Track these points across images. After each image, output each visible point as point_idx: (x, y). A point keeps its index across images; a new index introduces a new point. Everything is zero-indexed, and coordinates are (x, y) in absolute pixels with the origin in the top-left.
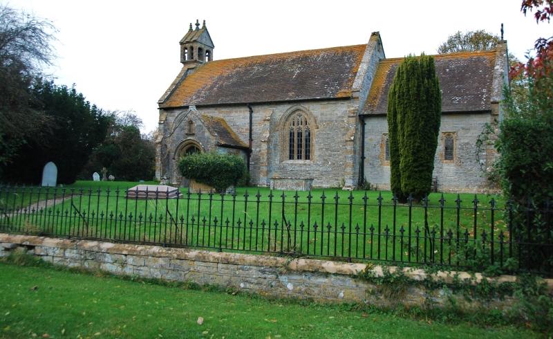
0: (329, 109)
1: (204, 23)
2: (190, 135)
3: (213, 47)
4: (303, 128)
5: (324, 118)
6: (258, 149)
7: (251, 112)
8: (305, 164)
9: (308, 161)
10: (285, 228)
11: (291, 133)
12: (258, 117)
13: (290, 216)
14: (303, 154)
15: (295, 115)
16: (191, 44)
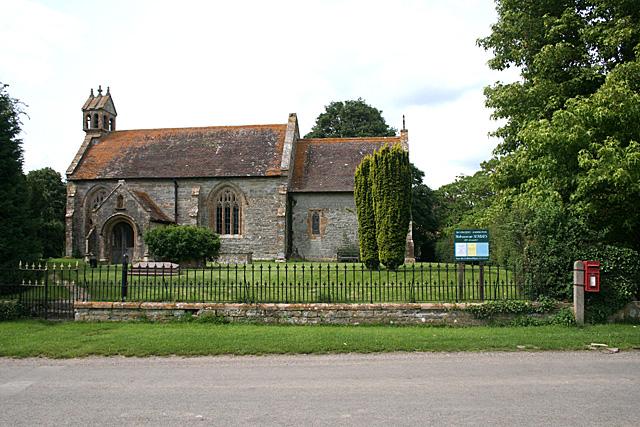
4: (231, 205)
7: (177, 187)
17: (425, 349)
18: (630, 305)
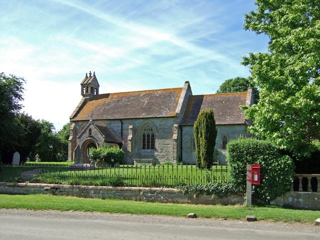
1: (94, 74)
4: (150, 133)
7: (122, 123)
17: (6, 194)
18: (288, 194)
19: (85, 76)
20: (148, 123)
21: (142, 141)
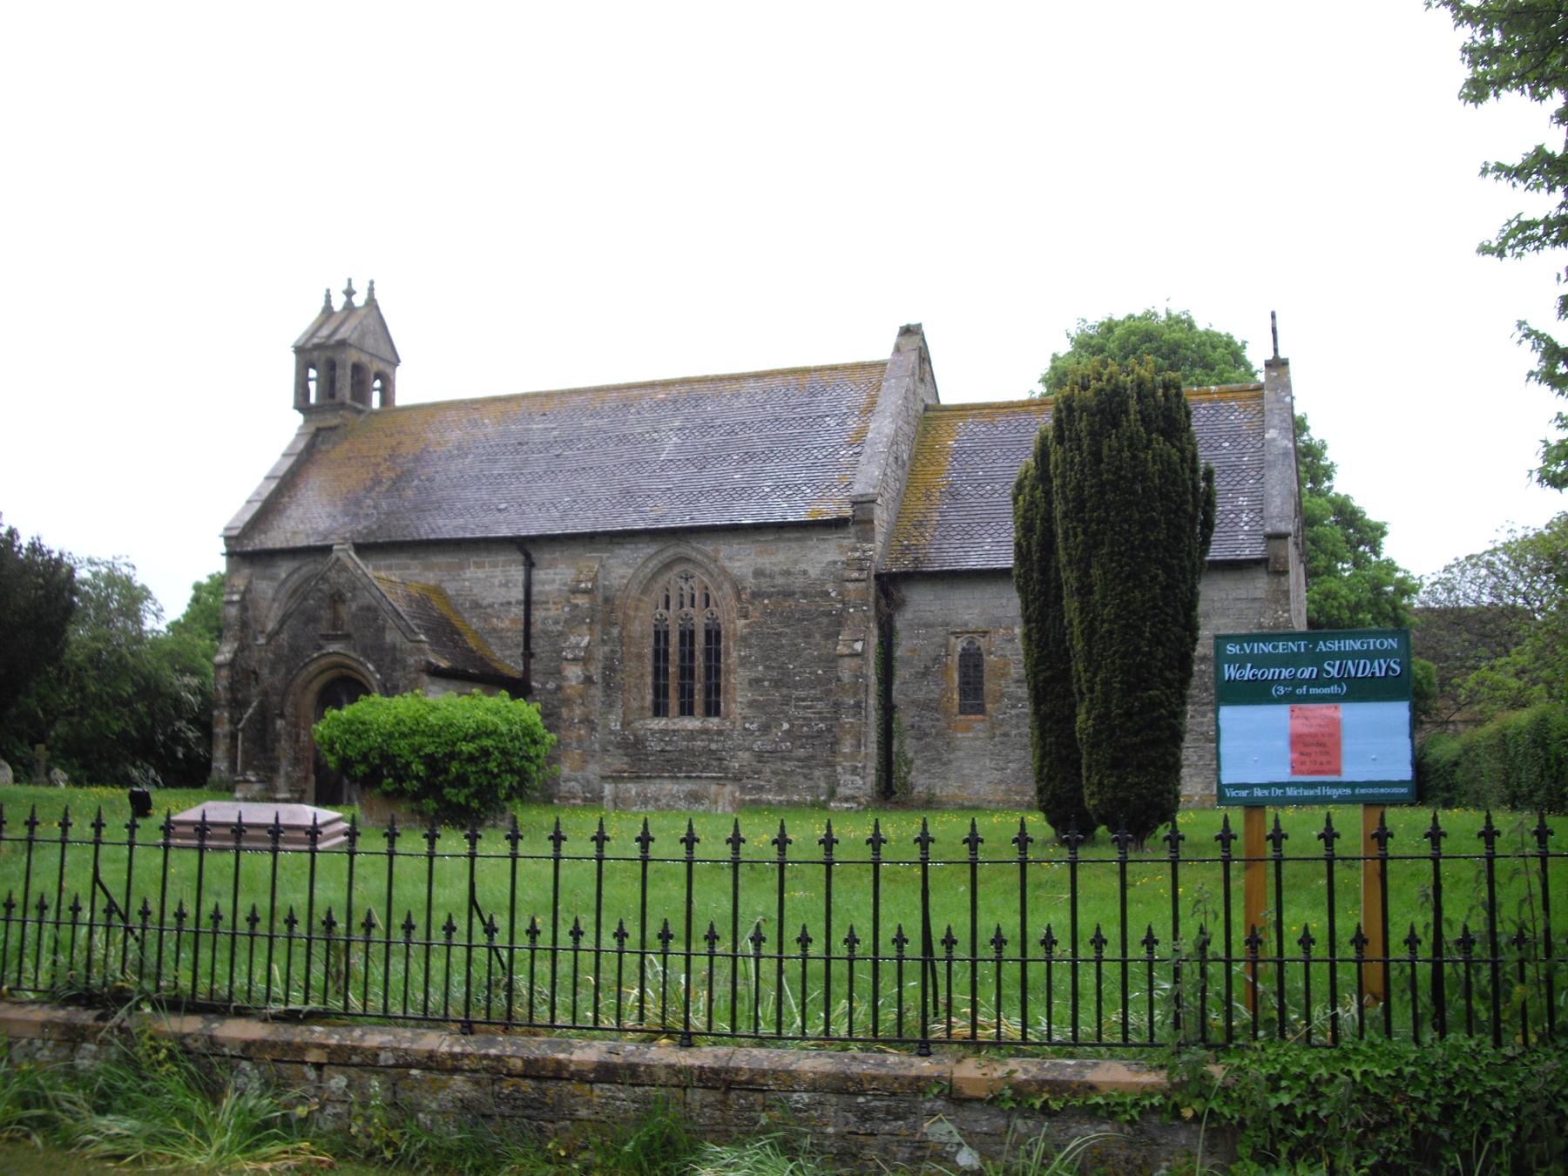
0: (781, 557)
1: (371, 290)
2: (335, 638)
3: (395, 361)
5: (765, 584)
6: (551, 685)
7: (530, 565)
8: (705, 731)
9: (716, 720)
10: (480, 937)
11: (657, 633)
12: (553, 581)
13: (712, 904)
14: (699, 698)
15: (671, 575)
16: (329, 354)
19: (322, 304)
20: (688, 560)
21: (649, 668)
